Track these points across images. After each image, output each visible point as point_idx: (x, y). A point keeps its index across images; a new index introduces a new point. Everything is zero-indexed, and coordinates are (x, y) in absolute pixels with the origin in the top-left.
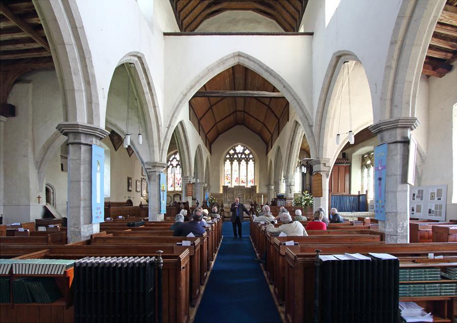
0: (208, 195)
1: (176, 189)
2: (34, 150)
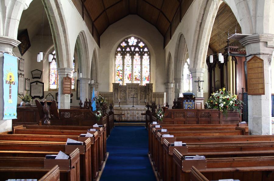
0: (95, 93)
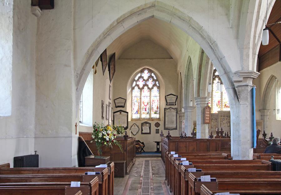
1: (143, 116)
2: (75, 58)
